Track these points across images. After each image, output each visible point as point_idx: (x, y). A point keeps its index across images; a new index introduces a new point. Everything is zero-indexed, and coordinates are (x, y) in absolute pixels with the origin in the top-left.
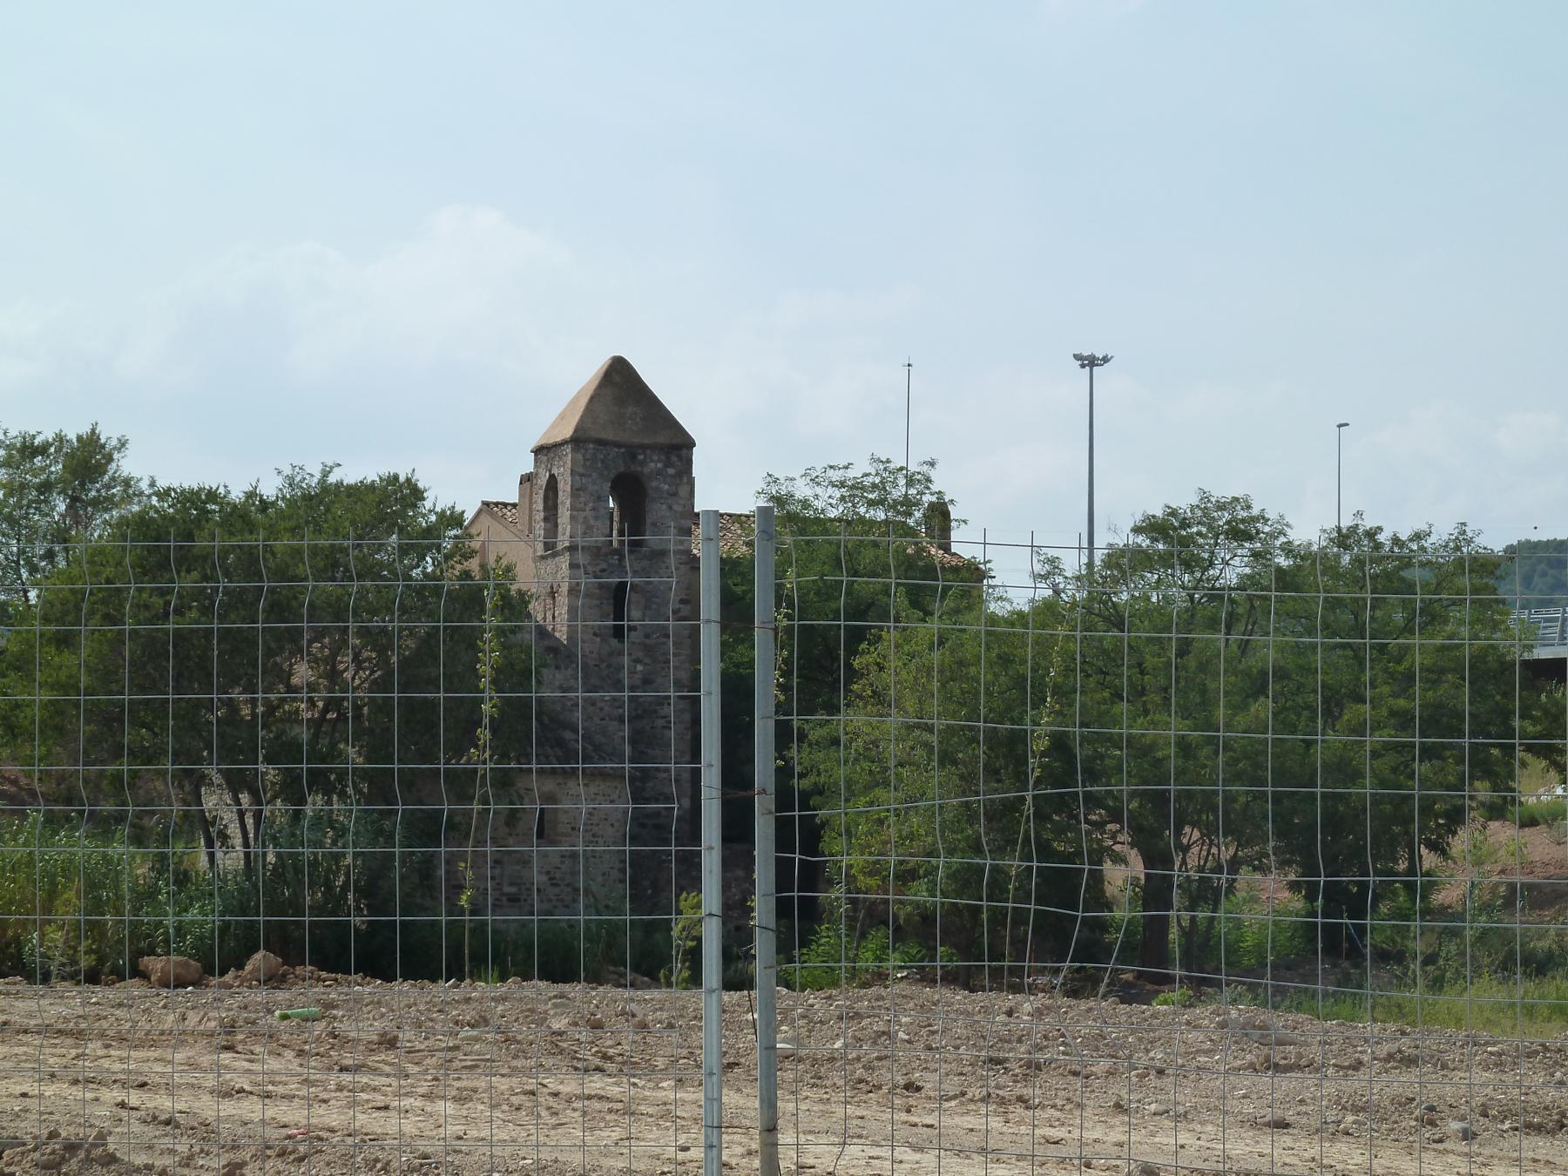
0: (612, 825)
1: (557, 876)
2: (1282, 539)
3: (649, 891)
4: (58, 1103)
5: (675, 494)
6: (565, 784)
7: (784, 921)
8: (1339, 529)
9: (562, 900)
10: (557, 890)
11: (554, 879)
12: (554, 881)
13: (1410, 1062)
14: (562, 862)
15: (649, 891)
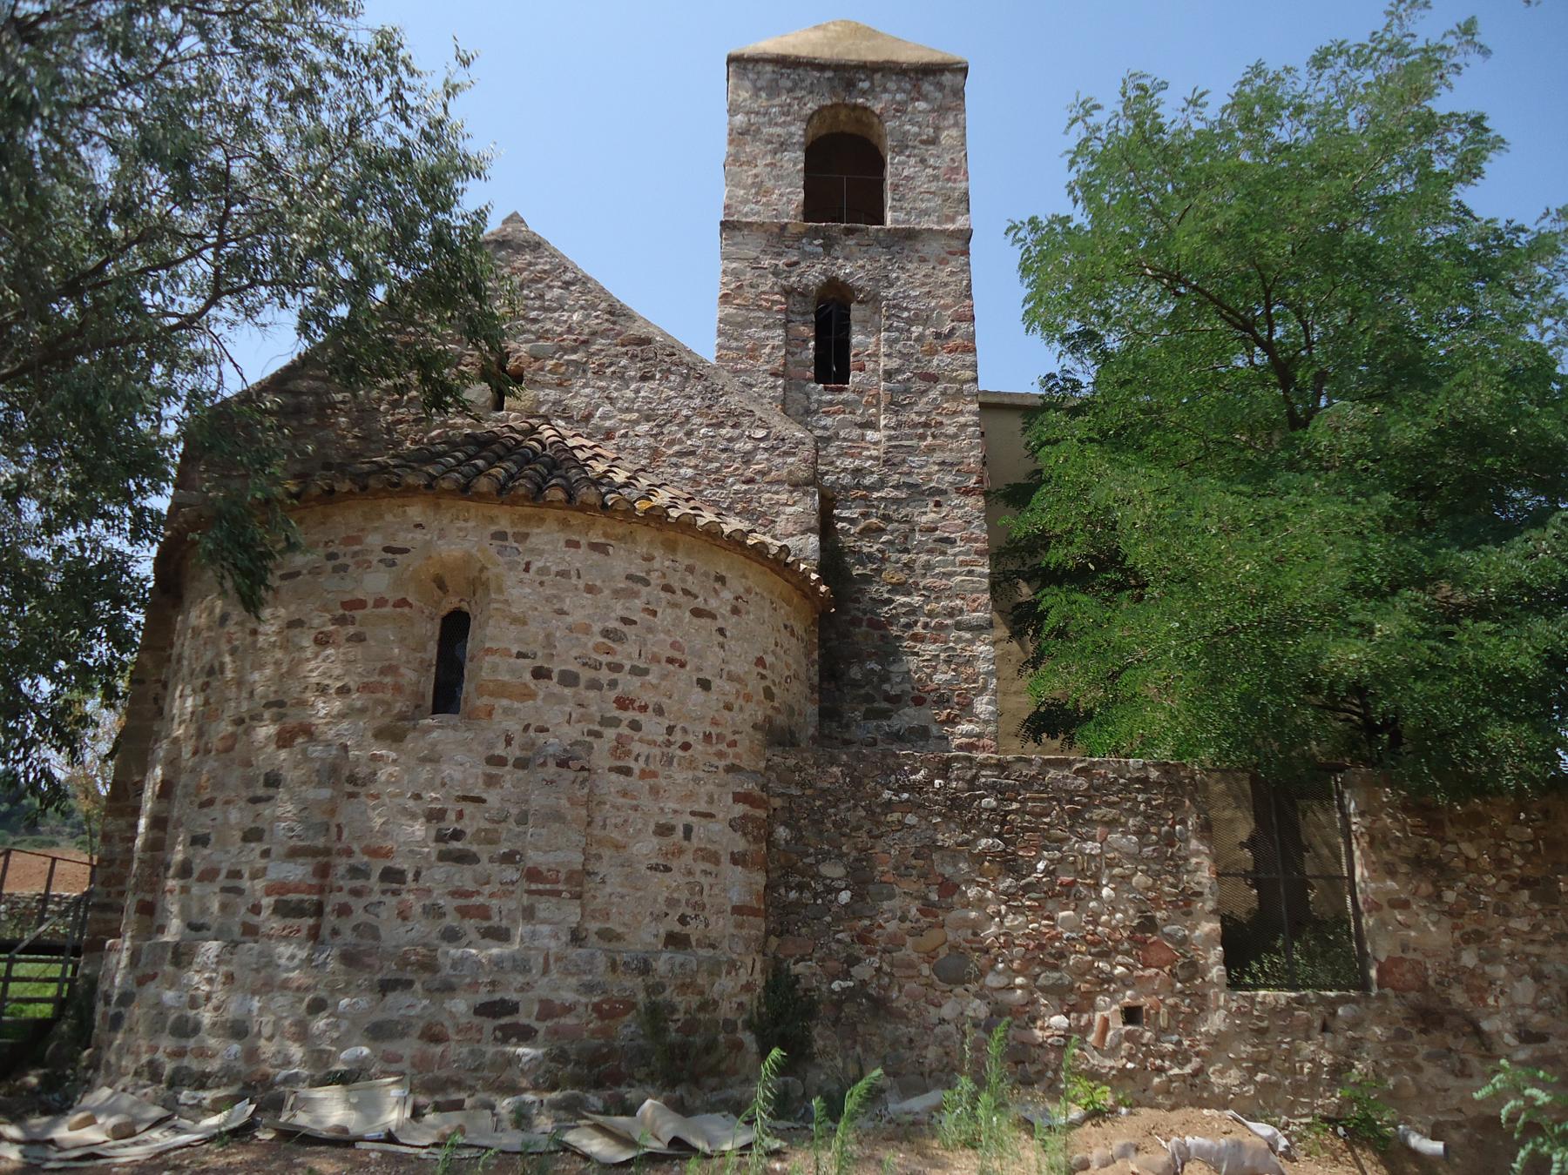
0: (705, 685)
2: (1342, 687)
3: (845, 897)
5: (933, 141)
6: (524, 537)
9: (483, 912)
10: (464, 876)
11: (457, 835)
14: (491, 781)
15: (845, 897)
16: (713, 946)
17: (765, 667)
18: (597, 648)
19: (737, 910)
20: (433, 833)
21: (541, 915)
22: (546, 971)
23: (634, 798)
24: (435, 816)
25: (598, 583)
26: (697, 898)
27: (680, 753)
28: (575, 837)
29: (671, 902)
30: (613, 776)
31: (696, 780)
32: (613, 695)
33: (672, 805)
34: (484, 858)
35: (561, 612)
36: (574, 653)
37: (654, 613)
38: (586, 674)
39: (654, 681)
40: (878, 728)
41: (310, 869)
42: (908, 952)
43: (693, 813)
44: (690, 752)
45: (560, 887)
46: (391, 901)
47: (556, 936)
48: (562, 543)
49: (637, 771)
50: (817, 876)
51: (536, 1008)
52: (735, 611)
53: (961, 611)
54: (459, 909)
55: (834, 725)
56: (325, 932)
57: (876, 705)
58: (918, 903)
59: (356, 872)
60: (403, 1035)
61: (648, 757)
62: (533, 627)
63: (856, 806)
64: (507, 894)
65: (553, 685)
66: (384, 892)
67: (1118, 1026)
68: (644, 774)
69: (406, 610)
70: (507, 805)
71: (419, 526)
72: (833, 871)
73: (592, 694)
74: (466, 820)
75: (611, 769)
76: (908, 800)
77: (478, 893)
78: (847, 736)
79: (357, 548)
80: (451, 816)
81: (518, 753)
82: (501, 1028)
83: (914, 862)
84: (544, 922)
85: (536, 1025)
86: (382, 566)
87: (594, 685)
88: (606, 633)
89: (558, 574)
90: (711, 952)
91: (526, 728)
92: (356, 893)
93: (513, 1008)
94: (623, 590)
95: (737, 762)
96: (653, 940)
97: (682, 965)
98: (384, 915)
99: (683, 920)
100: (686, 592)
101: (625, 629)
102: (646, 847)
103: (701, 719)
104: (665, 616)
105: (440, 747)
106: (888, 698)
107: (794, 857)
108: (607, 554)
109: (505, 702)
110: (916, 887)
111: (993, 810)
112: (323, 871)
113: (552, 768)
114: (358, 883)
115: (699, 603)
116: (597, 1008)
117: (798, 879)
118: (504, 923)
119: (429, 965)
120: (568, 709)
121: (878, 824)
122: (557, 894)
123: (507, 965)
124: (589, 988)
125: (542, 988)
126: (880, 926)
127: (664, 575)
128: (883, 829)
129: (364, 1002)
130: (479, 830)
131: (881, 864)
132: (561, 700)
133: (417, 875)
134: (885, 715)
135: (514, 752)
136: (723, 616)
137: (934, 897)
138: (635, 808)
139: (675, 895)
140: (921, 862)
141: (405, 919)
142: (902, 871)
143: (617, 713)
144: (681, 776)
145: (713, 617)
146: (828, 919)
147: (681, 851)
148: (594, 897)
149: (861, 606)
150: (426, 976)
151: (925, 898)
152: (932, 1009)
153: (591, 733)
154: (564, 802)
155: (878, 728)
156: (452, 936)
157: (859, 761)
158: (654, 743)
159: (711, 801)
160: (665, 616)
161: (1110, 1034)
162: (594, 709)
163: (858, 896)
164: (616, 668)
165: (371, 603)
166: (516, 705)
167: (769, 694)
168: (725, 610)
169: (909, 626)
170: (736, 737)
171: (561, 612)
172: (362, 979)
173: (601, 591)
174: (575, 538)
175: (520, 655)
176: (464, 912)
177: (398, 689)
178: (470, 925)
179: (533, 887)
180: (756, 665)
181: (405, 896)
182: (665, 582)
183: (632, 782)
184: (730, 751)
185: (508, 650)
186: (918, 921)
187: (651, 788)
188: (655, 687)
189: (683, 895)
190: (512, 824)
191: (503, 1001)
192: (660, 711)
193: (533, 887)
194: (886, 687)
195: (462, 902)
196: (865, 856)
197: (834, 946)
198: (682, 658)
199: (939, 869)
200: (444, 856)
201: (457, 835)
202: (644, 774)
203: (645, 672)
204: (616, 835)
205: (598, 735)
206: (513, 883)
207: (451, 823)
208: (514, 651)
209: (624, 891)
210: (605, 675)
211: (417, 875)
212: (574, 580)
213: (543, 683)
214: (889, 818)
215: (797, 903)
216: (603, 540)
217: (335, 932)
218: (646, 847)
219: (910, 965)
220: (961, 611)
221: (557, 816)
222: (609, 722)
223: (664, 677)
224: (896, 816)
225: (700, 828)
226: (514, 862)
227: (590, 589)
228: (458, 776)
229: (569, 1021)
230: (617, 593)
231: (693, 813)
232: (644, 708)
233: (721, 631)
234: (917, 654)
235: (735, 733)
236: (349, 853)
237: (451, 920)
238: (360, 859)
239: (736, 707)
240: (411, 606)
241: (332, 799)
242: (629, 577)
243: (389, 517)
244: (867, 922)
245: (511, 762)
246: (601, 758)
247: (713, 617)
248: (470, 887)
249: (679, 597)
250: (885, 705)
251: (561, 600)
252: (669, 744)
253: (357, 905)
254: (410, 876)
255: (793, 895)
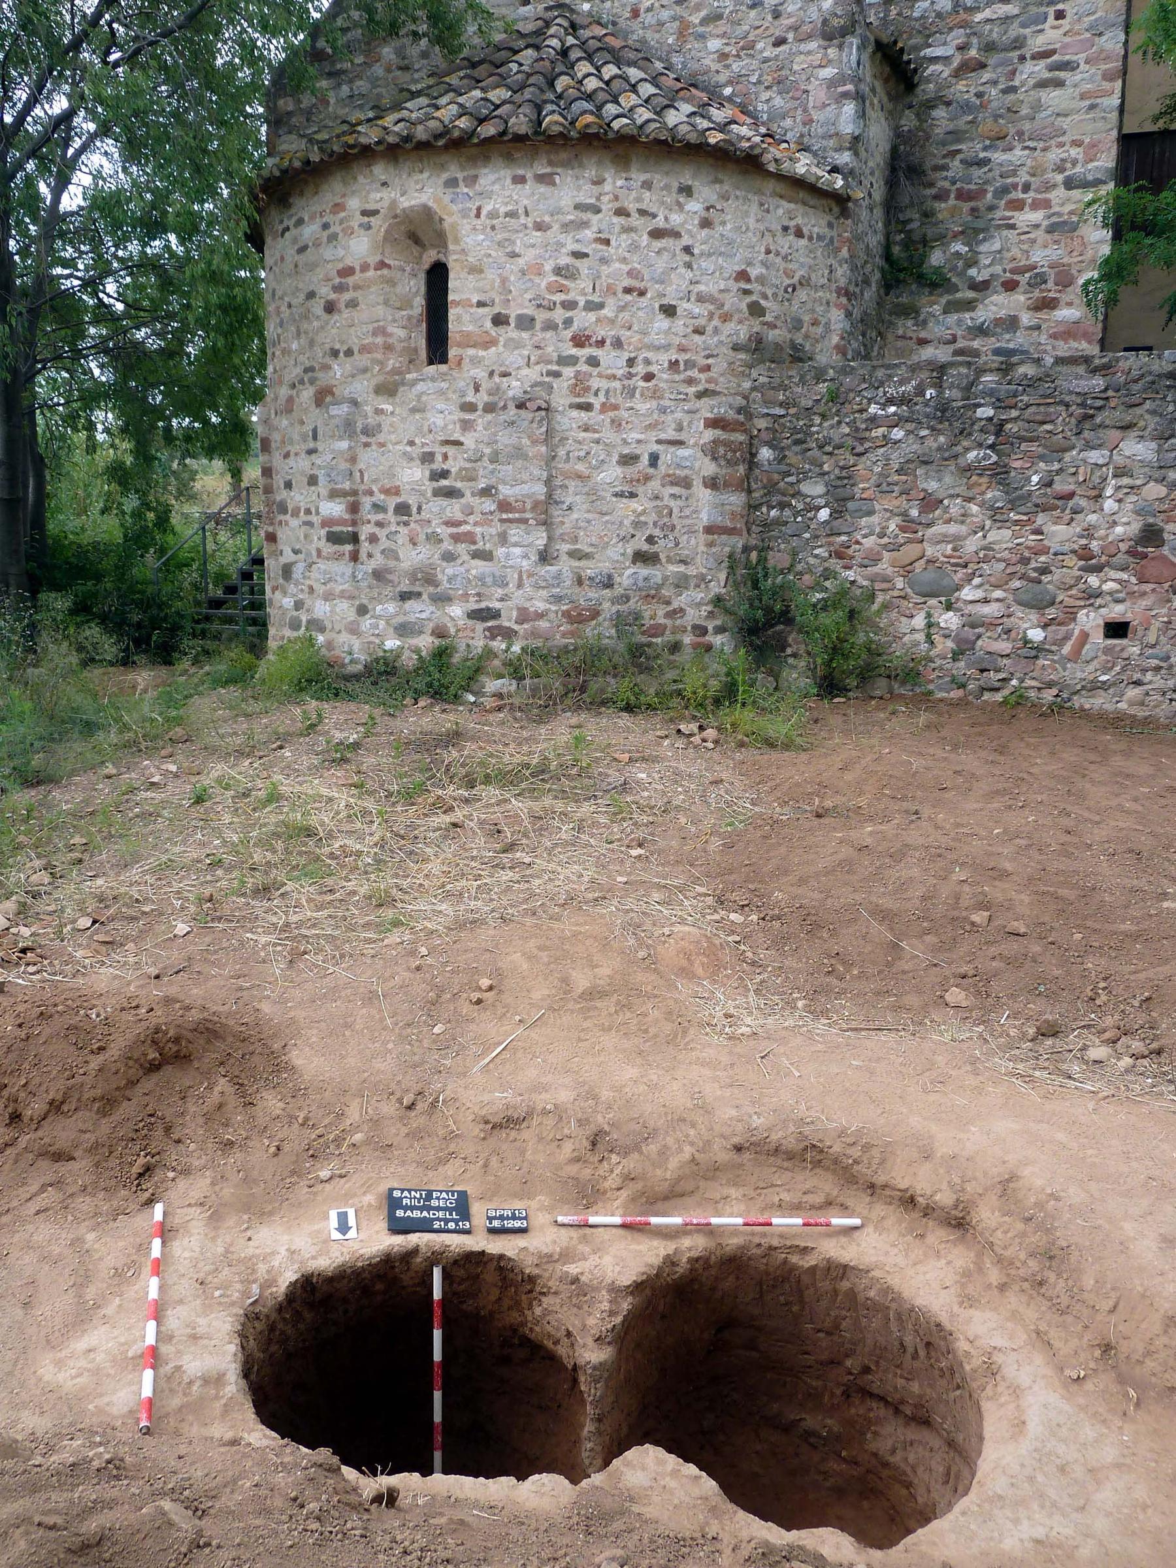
0: (669, 311)
1: (453, 466)
3: (824, 514)
4: (694, 727)
7: (480, 650)
8: (713, 1289)
9: (469, 538)
10: (453, 508)
11: (444, 474)
12: (444, 483)
13: (858, 64)
14: (466, 426)
15: (824, 514)
16: (683, 562)
17: (749, 280)
18: (549, 288)
19: (709, 530)
20: (427, 473)
21: (513, 539)
22: (520, 585)
23: (596, 431)
24: (428, 458)
25: (547, 219)
26: (666, 520)
27: (642, 384)
28: (536, 472)
29: (637, 524)
30: (575, 413)
31: (663, 411)
32: (568, 334)
33: (636, 436)
34: (468, 493)
35: (514, 255)
36: (528, 296)
37: (607, 242)
38: (541, 316)
39: (611, 315)
40: (959, 322)
41: (343, 507)
42: (884, 567)
43: (659, 442)
44: (654, 382)
45: (528, 515)
46: (404, 530)
47: (525, 556)
48: (509, 181)
49: (597, 406)
50: (797, 494)
51: (515, 614)
52: (706, 223)
53: (1074, 163)
54: (453, 536)
55: (910, 323)
56: (363, 555)
57: (959, 295)
58: (898, 520)
59: (377, 508)
60: (421, 632)
61: (607, 392)
62: (491, 275)
63: (839, 422)
64: (488, 523)
65: (511, 332)
66: (398, 524)
67: (1098, 638)
68: (604, 408)
69: (385, 271)
70: (481, 446)
71: (384, 184)
72: (814, 489)
73: (549, 334)
74: (450, 462)
75: (571, 406)
76: (895, 414)
77: (466, 522)
78: (923, 335)
79: (343, 214)
80: (439, 458)
81: (486, 398)
82: (489, 629)
83: (896, 478)
84: (516, 545)
85: (516, 627)
86: (362, 232)
87: (550, 326)
88: (558, 271)
89: (507, 215)
90: (682, 568)
91: (491, 374)
92: (380, 524)
93: (496, 615)
94: (572, 222)
95: (712, 386)
96: (621, 558)
97: (645, 579)
98: (400, 542)
99: (650, 540)
100: (642, 212)
101: (578, 263)
102: (612, 474)
103: (666, 347)
104: (621, 243)
105: (424, 398)
106: (975, 286)
107: (776, 477)
108: (554, 184)
109: (471, 352)
110: (896, 503)
111: (990, 419)
112: (354, 508)
113: (512, 411)
114: (380, 517)
115: (660, 222)
116: (567, 614)
117: (780, 498)
118: (488, 547)
119: (431, 580)
120: (526, 353)
121: (862, 440)
122: (525, 521)
123: (489, 580)
124: (558, 599)
125: (518, 598)
126: (858, 543)
127: (616, 198)
128: (867, 445)
129: (391, 607)
130: (461, 469)
131: (862, 481)
132: (518, 345)
133: (419, 509)
134: (969, 305)
135: (482, 398)
136: (689, 232)
137: (914, 513)
138: (598, 442)
139: (642, 518)
140: (904, 478)
141: (415, 544)
142: (883, 487)
143: (574, 351)
144: (644, 406)
145: (677, 235)
146: (807, 535)
147: (648, 478)
148: (563, 523)
149: (950, 174)
150: (431, 589)
151: (905, 514)
152: (903, 619)
153: (549, 373)
154: (526, 441)
155: (959, 322)
156: (449, 557)
157: (846, 374)
158: (614, 377)
159: (680, 429)
160: (621, 243)
161: (1087, 647)
162: (550, 349)
163: (836, 514)
164: (570, 305)
165: (358, 268)
166: (481, 353)
167: (756, 310)
168: (693, 225)
169: (1005, 190)
170: (710, 361)
171: (514, 255)
172: (388, 591)
173: (549, 227)
174: (520, 172)
175: (481, 304)
176: (456, 538)
177: (388, 348)
178: (462, 548)
179: (504, 516)
180: (737, 279)
181: (412, 525)
182: (617, 205)
183: (593, 417)
184: (702, 376)
185: (469, 300)
186: (897, 536)
187: (613, 421)
188: (612, 322)
189: (651, 518)
190: (486, 462)
191: (488, 609)
192: (618, 344)
193: (504, 516)
194: (973, 272)
195: (454, 530)
196: (847, 476)
197: (812, 561)
198: (642, 285)
199: (922, 485)
200: (437, 493)
201: (444, 474)
202: (604, 408)
203: (601, 306)
204: (580, 467)
205: (557, 375)
206: (491, 513)
207: (438, 465)
208: (475, 301)
209: (590, 516)
210: (559, 315)
211: (419, 509)
212: (523, 220)
213: (501, 330)
214: (873, 434)
215: (778, 522)
216: (548, 170)
217: (370, 556)
218: (612, 474)
219: (886, 579)
220: (1074, 163)
221: (518, 453)
222: (565, 361)
223: (622, 309)
224: (881, 431)
225: (668, 456)
226: (491, 495)
227: (540, 227)
228: (440, 422)
229: (543, 624)
230: (566, 227)
231: (659, 442)
232: (601, 343)
233: (687, 250)
234: (1012, 227)
235: (707, 357)
236: (371, 493)
237: (447, 545)
238: (379, 497)
239: (709, 329)
240: (389, 267)
241: (350, 448)
242: (577, 207)
243: (361, 179)
244: (844, 538)
245: (480, 407)
246: (561, 398)
247: (677, 235)
248: (459, 516)
249: (635, 220)
250: (971, 294)
251: (513, 243)
252: (630, 376)
253: (381, 533)
254: (414, 510)
255: (774, 513)
